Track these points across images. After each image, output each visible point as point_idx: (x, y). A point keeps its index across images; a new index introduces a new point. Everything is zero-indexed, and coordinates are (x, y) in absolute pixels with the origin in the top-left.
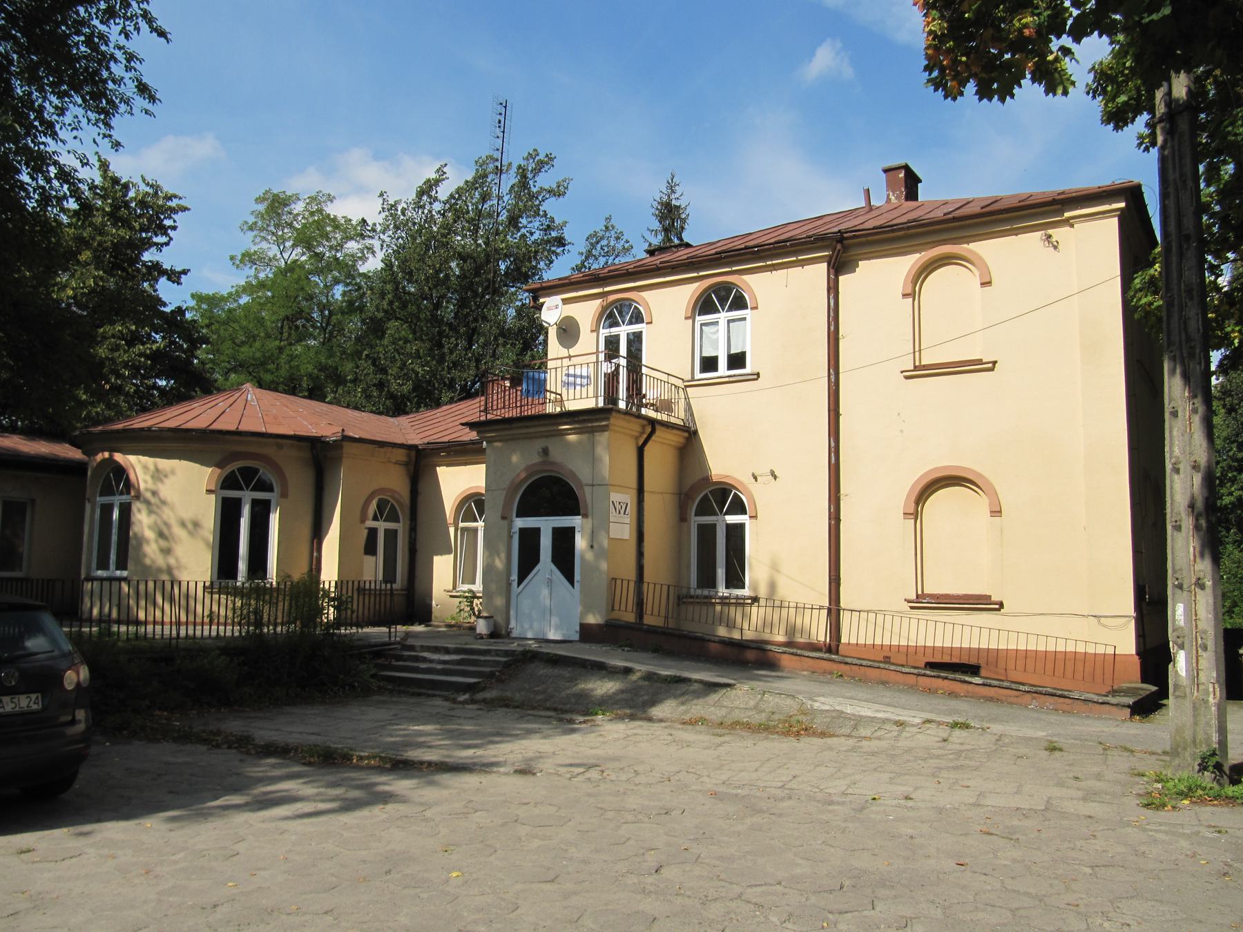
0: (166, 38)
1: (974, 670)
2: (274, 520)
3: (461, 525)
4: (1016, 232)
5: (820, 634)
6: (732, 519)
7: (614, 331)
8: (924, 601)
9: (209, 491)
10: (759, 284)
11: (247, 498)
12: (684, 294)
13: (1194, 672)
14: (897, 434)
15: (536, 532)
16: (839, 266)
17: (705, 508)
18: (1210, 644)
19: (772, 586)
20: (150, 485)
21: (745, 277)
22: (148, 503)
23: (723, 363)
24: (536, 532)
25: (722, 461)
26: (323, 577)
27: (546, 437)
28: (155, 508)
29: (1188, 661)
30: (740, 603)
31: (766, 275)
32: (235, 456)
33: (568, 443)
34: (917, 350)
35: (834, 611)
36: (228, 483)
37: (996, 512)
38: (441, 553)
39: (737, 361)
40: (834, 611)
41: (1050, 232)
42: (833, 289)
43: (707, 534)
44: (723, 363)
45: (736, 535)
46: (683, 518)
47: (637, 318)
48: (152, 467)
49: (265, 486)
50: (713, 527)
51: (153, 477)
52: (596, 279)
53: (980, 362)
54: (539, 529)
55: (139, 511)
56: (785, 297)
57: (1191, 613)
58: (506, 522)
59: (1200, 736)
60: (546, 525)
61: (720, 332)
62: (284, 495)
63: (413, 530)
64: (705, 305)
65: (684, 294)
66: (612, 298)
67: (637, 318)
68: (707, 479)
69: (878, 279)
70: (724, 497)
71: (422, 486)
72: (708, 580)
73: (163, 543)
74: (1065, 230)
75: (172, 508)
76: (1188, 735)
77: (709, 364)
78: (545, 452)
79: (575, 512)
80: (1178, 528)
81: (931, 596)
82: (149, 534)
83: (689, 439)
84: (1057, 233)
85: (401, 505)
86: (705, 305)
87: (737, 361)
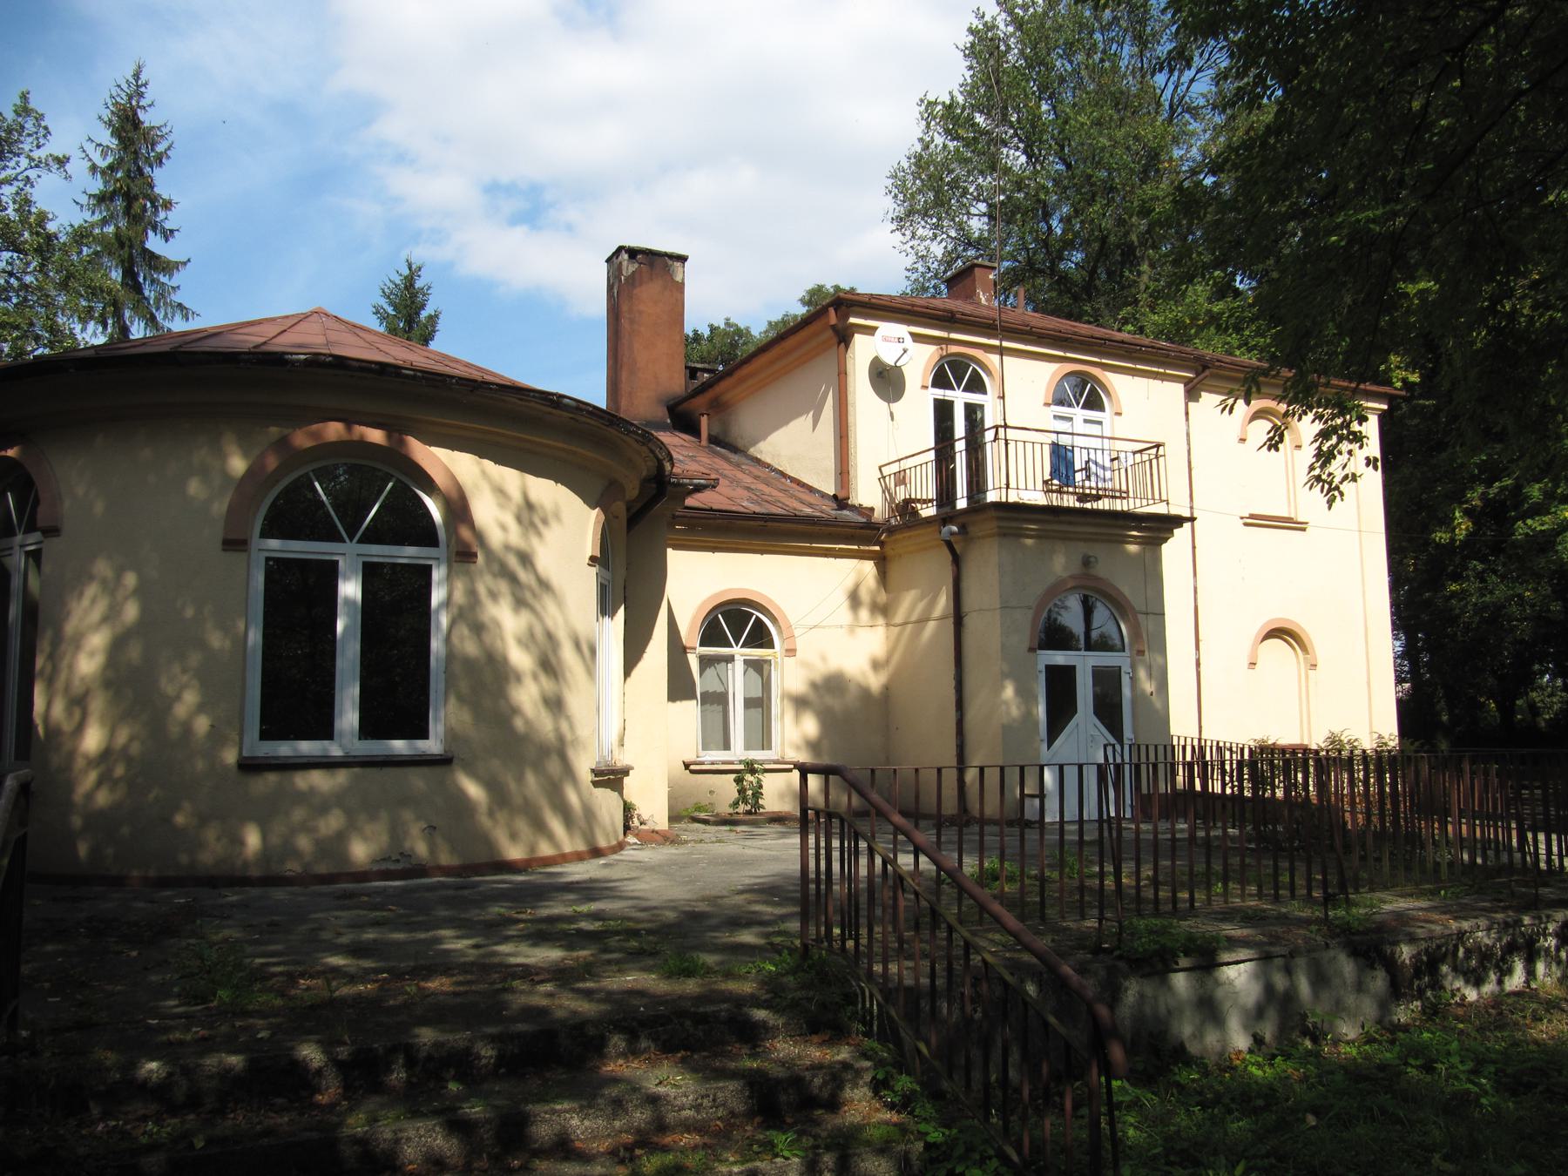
5: (934, 811)
7: (948, 394)
20: (515, 536)
26: (1175, 730)
27: (1085, 540)
28: (528, 596)
33: (1128, 555)
48: (516, 495)
51: (519, 519)
52: (949, 320)
54: (1073, 668)
55: (494, 596)
66: (954, 349)
67: (976, 385)
73: (547, 684)
75: (560, 603)
82: (520, 659)
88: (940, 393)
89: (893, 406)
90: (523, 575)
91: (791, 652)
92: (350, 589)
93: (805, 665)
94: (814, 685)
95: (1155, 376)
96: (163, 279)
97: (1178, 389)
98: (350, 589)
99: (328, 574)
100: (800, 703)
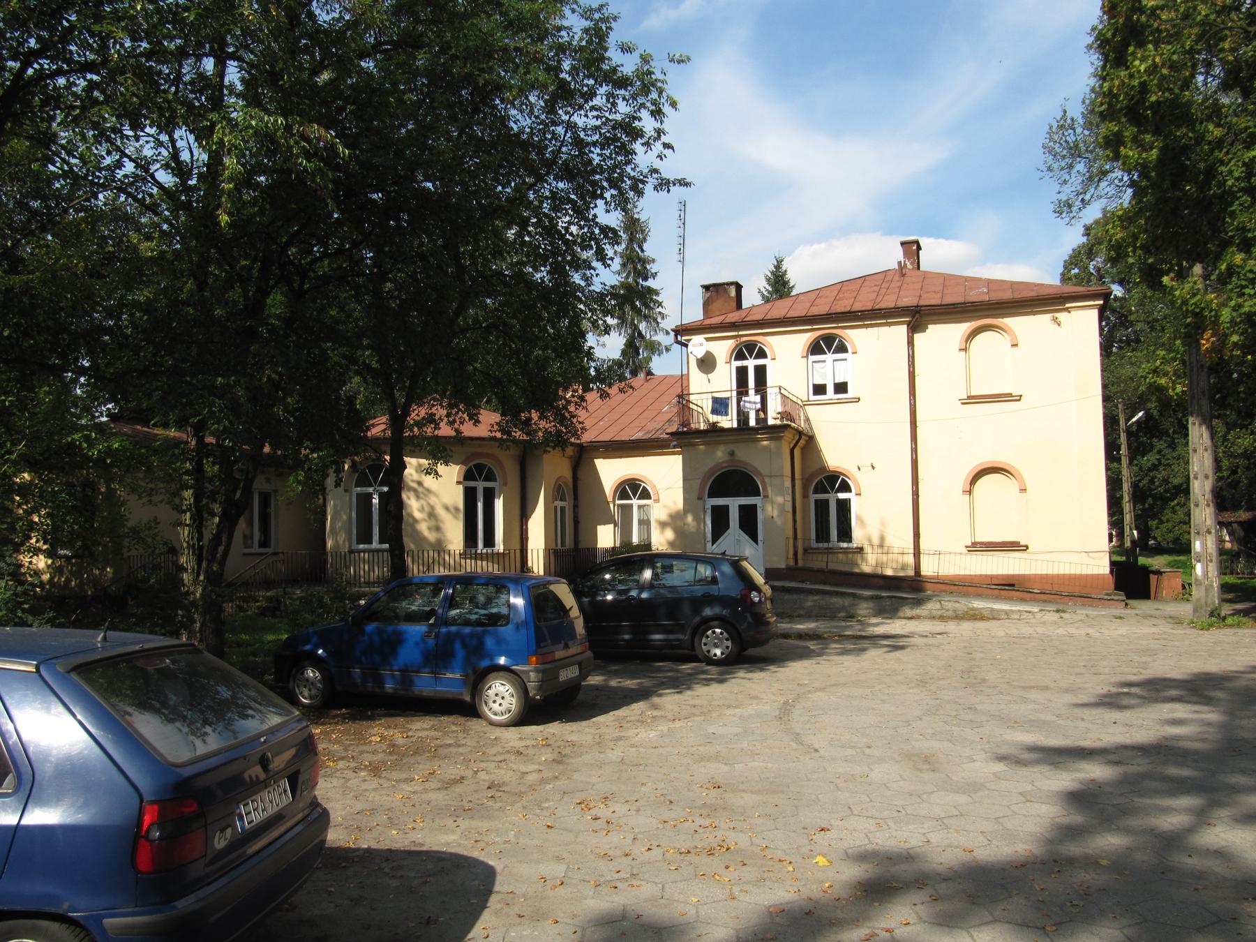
0: (778, 267)
1: (1013, 585)
2: (499, 504)
3: (618, 502)
4: (1034, 313)
6: (842, 496)
7: (745, 363)
8: (978, 547)
9: (458, 483)
10: (855, 336)
11: (480, 485)
12: (803, 339)
13: (1206, 573)
14: (955, 441)
15: (726, 508)
16: (916, 327)
17: (820, 488)
18: (1214, 559)
19: (882, 538)
21: (847, 331)
22: (415, 490)
23: (830, 389)
24: (726, 508)
25: (834, 456)
29: (1203, 567)
30: (846, 551)
31: (863, 330)
32: (474, 455)
34: (968, 386)
35: (917, 553)
36: (468, 476)
37: (1023, 490)
38: (604, 524)
39: (841, 388)
40: (917, 553)
41: (1057, 315)
42: (911, 343)
43: (822, 507)
44: (830, 389)
45: (844, 507)
46: (805, 496)
47: (762, 354)
49: (490, 477)
50: (826, 502)
52: (733, 326)
53: (1010, 395)
54: (727, 507)
56: (875, 349)
57: (1204, 545)
58: (701, 502)
59: (1209, 601)
60: (734, 504)
61: (828, 369)
62: (505, 484)
63: (576, 507)
64: (815, 349)
65: (803, 339)
67: (762, 354)
68: (824, 469)
69: (942, 337)
70: (834, 481)
71: (580, 473)
72: (823, 534)
74: (1066, 314)
75: (436, 496)
76: (1203, 601)
77: (819, 389)
78: (732, 454)
79: (756, 493)
80: (1197, 505)
81: (981, 543)
82: (417, 515)
83: (806, 442)
84: (1061, 316)
85: (567, 485)
86: (815, 349)
87: (841, 388)
88: (739, 363)
89: (710, 376)
90: (420, 489)
91: (657, 501)
92: (376, 501)
93: (665, 506)
94: (671, 516)
95: (872, 326)
96: (643, 326)
97: (903, 329)
98: (376, 501)
99: (370, 496)
100: (663, 525)
